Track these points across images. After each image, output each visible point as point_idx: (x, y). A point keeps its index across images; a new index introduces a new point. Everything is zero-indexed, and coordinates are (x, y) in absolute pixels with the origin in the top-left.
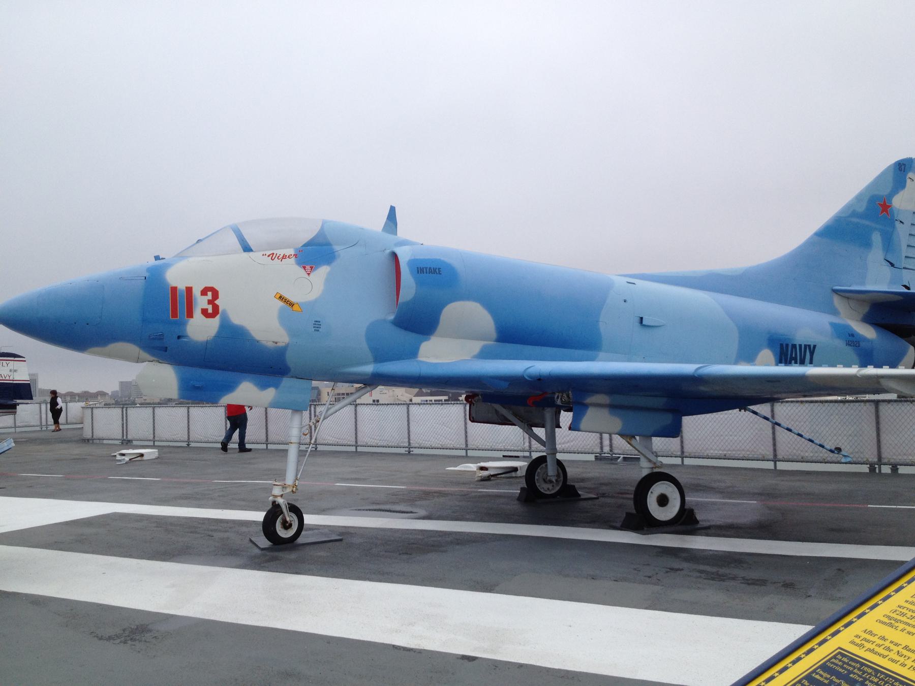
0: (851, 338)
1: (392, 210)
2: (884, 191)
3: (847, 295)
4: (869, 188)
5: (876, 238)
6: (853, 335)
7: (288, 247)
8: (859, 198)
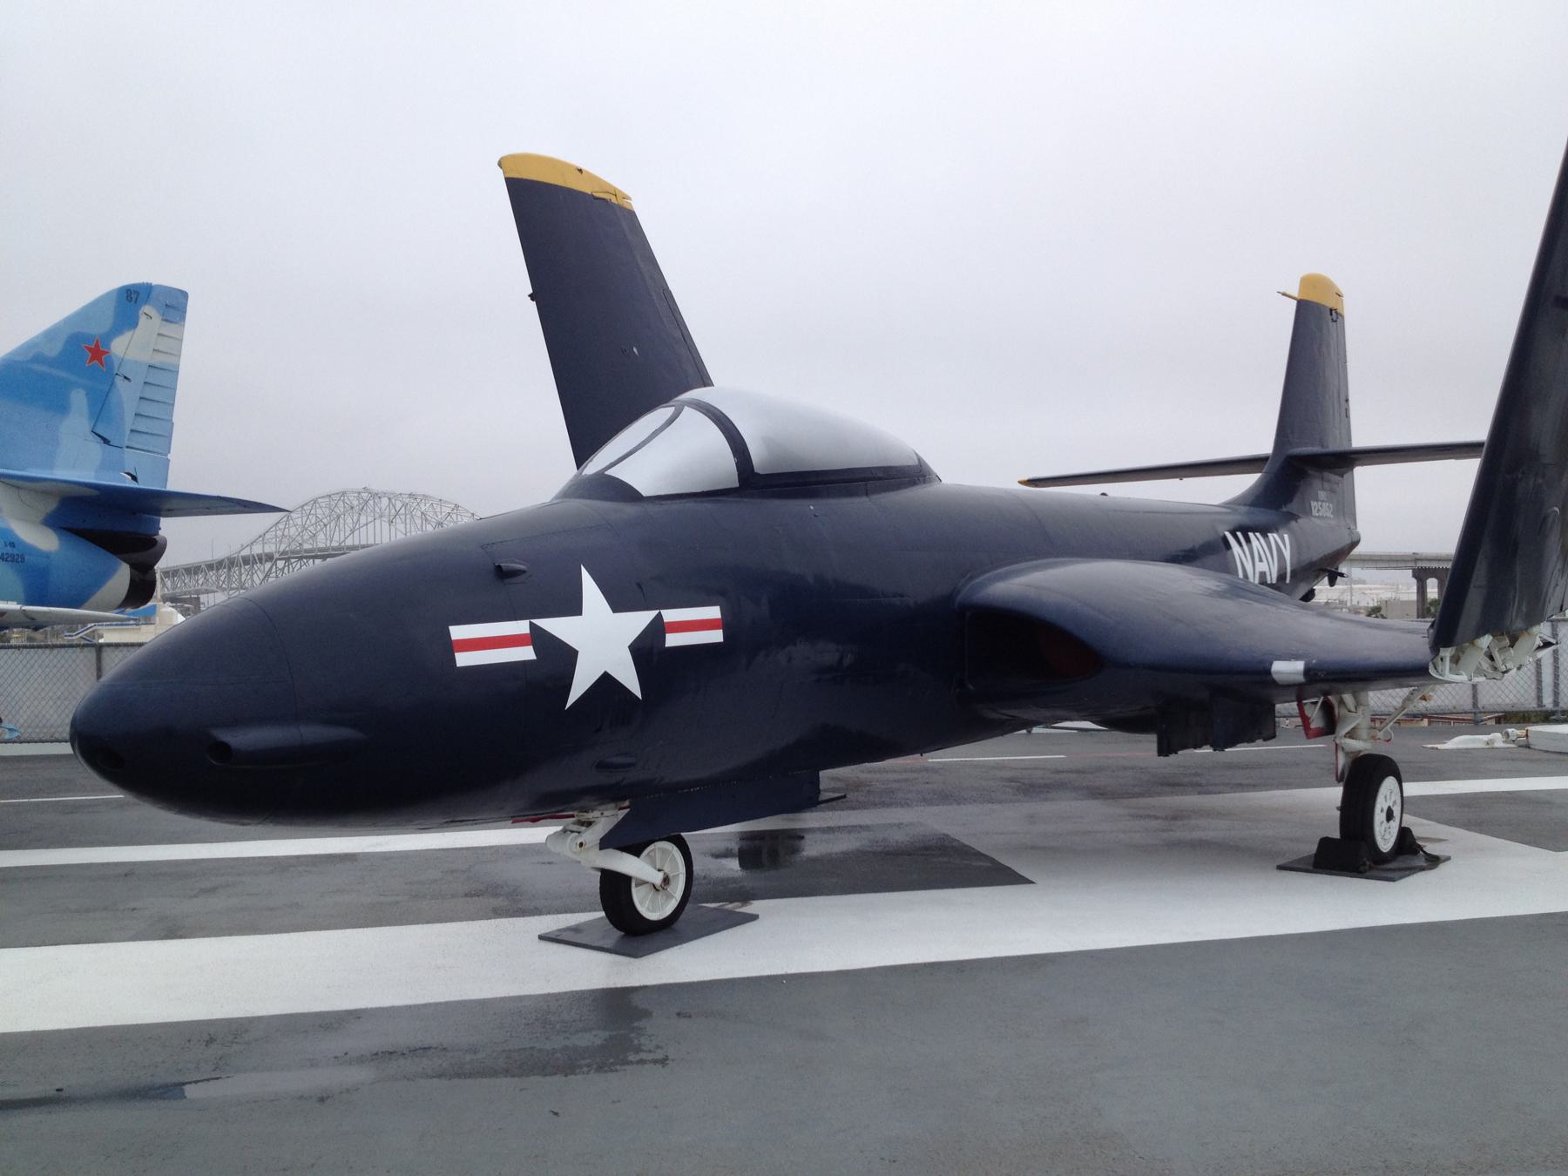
0: (9, 550)
1: (541, 938)
2: (97, 329)
3: (20, 483)
4: (68, 321)
5: (79, 399)
6: (12, 545)
7: (1296, 657)
8: (50, 335)
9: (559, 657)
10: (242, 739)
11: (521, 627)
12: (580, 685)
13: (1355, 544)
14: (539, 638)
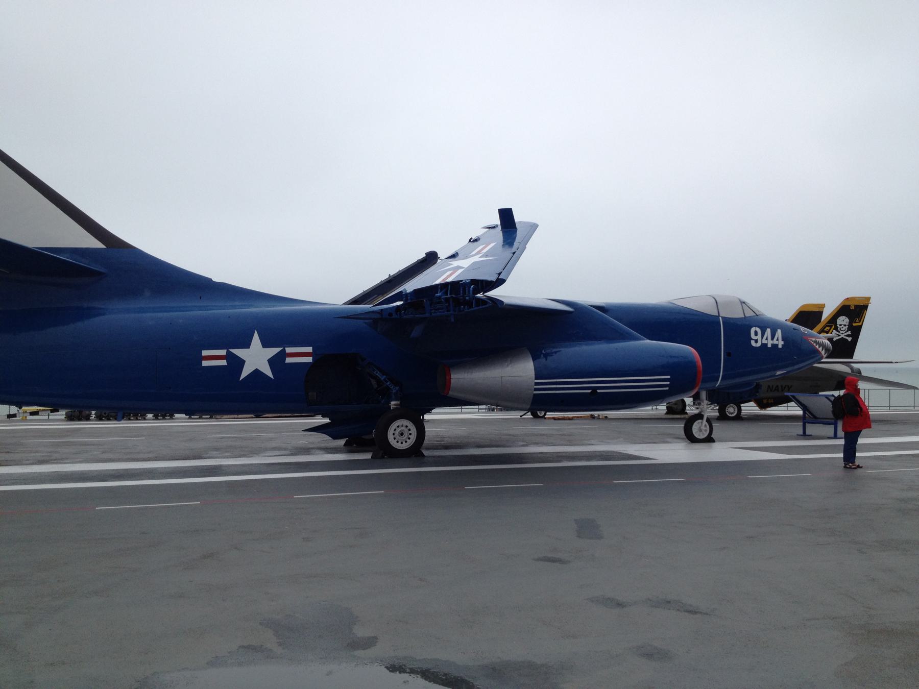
7: (549, 418)
9: (239, 363)
10: (183, 415)
11: (223, 352)
12: (245, 373)
13: (500, 282)
14: (230, 357)
